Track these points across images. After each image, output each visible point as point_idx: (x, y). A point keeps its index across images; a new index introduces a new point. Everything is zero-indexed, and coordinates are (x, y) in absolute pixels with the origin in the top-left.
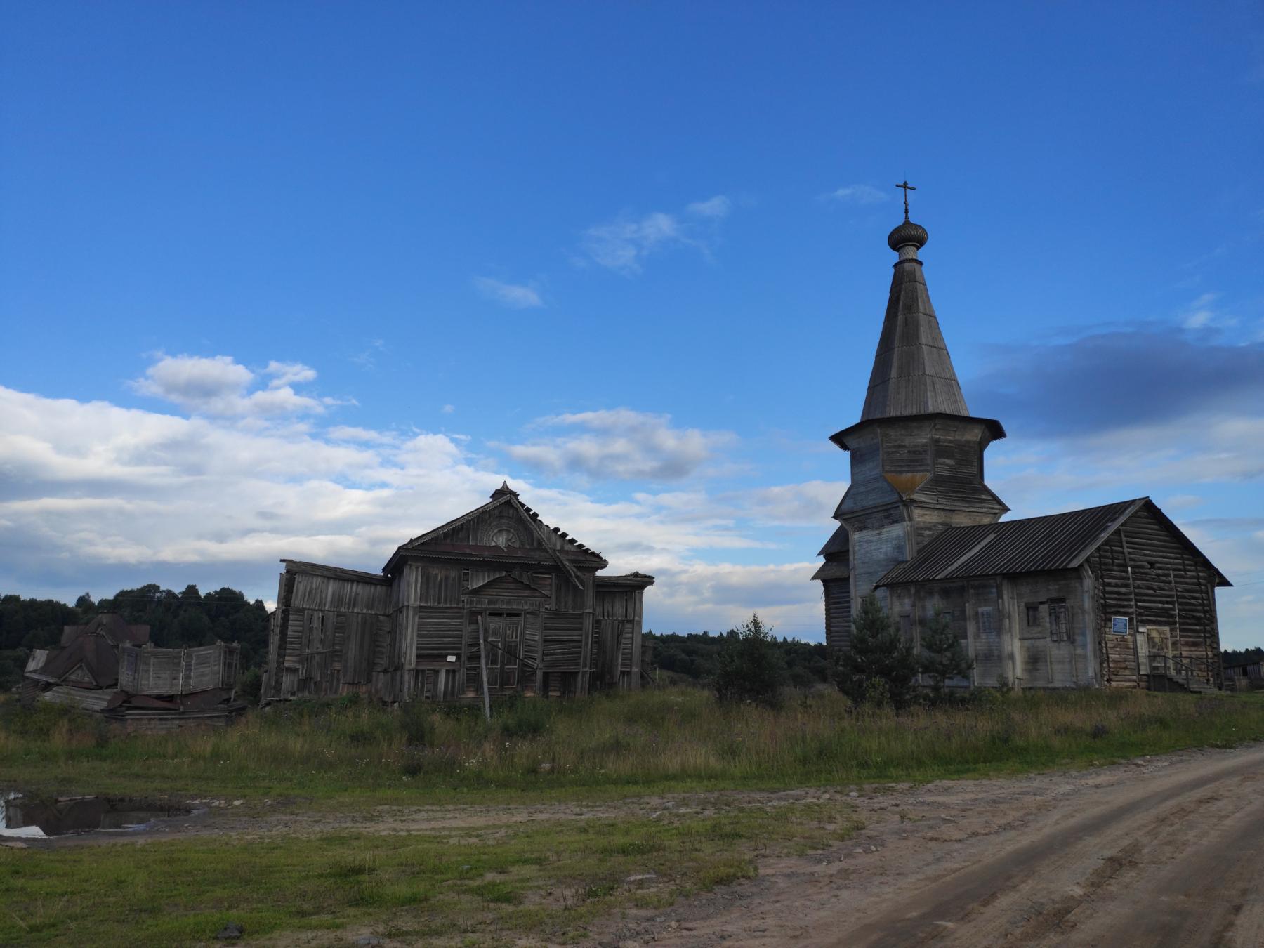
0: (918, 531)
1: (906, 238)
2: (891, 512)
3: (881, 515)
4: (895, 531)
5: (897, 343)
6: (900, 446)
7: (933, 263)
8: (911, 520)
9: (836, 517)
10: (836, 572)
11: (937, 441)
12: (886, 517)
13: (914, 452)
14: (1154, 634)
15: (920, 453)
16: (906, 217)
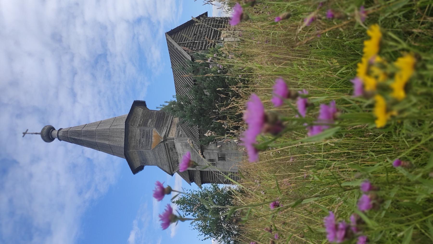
0: (179, 136)
1: (48, 135)
2: (170, 148)
3: (171, 152)
4: (178, 146)
5: (93, 140)
6: (140, 142)
7: (61, 124)
8: (173, 139)
9: (172, 175)
10: (198, 177)
11: (139, 125)
12: (172, 150)
13: (143, 135)
14: (225, 35)
15: (144, 133)
16: (39, 134)
